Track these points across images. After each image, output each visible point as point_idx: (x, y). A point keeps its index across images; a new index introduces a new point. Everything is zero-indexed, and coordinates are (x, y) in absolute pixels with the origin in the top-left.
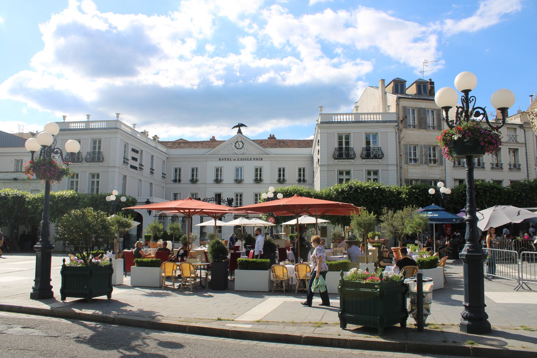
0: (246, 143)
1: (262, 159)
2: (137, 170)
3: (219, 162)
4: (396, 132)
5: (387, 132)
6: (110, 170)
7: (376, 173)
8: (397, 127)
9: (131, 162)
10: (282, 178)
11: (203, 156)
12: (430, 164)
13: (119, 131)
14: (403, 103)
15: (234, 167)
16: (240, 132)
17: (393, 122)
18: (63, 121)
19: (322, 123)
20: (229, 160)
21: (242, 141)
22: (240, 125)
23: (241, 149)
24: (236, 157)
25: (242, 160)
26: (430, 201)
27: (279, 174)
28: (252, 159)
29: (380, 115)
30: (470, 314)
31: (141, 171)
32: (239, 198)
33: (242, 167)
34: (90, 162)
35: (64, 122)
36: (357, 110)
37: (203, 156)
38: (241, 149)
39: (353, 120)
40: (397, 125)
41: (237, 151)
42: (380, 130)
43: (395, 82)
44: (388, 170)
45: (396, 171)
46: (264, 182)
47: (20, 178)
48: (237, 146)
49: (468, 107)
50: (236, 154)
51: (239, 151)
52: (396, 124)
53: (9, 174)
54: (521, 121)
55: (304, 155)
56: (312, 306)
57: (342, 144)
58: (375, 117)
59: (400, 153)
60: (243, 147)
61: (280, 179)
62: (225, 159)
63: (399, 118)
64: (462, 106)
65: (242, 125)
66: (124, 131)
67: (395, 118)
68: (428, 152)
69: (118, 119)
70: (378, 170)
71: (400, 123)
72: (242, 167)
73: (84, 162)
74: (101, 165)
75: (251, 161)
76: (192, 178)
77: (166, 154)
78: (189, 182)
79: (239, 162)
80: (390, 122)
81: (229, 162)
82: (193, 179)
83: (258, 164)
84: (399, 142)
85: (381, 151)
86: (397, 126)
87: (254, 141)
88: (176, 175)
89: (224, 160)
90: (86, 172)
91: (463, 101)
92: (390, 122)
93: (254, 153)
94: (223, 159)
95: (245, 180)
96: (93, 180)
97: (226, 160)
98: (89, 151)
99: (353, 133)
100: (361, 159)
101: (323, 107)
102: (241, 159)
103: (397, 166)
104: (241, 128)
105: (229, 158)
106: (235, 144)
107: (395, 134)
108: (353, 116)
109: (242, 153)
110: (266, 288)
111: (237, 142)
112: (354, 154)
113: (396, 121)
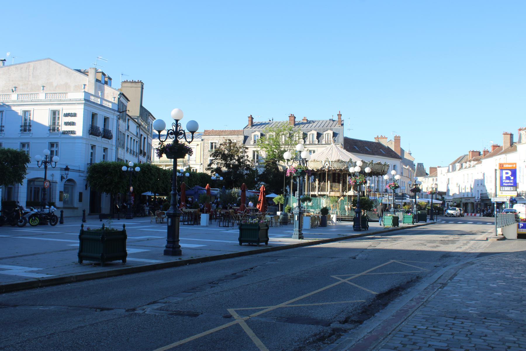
103: (116, 147)
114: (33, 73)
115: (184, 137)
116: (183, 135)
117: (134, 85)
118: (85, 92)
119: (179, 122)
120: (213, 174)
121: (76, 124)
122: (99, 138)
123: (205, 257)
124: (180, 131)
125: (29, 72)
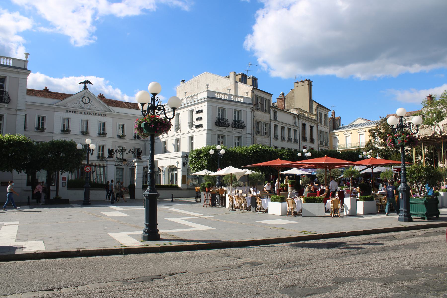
0: (92, 99)
1: (105, 115)
3: (67, 113)
5: (19, 78)
7: (223, 137)
10: (40, 126)
11: (52, 106)
12: (265, 136)
14: (256, 93)
15: (98, 121)
16: (85, 88)
20: (76, 112)
21: (89, 97)
23: (87, 104)
25: (88, 114)
27: (38, 122)
28: (97, 115)
30: (149, 230)
32: (101, 149)
36: (27, 57)
37: (52, 106)
38: (87, 104)
41: (83, 105)
45: (251, 138)
46: (107, 136)
48: (84, 101)
49: (402, 123)
50: (83, 108)
51: (85, 106)
52: (252, 106)
54: (297, 113)
55: (136, 116)
56: (303, 216)
58: (6, 62)
59: (253, 126)
60: (89, 102)
61: (39, 127)
62: (72, 111)
64: (399, 123)
67: (250, 102)
68: (265, 127)
70: (225, 135)
75: (96, 116)
78: (35, 130)
80: (248, 104)
83: (103, 119)
84: (253, 119)
85: (9, 95)
88: (39, 123)
89: (71, 112)
91: (400, 121)
92: (248, 104)
93: (99, 109)
99: (10, 77)
101: (29, 54)
102: (87, 114)
103: (252, 135)
104: (87, 84)
105: (76, 111)
106: (82, 99)
107: (251, 113)
109: (89, 108)
110: (325, 207)
111: (84, 97)
112: (229, 124)
114: (197, 86)
115: (163, 112)
116: (162, 110)
117: (303, 84)
118: (208, 91)
119: (156, 96)
120: (382, 153)
121: (203, 119)
122: (230, 129)
123: (114, 248)
124: (158, 105)
125: (195, 85)
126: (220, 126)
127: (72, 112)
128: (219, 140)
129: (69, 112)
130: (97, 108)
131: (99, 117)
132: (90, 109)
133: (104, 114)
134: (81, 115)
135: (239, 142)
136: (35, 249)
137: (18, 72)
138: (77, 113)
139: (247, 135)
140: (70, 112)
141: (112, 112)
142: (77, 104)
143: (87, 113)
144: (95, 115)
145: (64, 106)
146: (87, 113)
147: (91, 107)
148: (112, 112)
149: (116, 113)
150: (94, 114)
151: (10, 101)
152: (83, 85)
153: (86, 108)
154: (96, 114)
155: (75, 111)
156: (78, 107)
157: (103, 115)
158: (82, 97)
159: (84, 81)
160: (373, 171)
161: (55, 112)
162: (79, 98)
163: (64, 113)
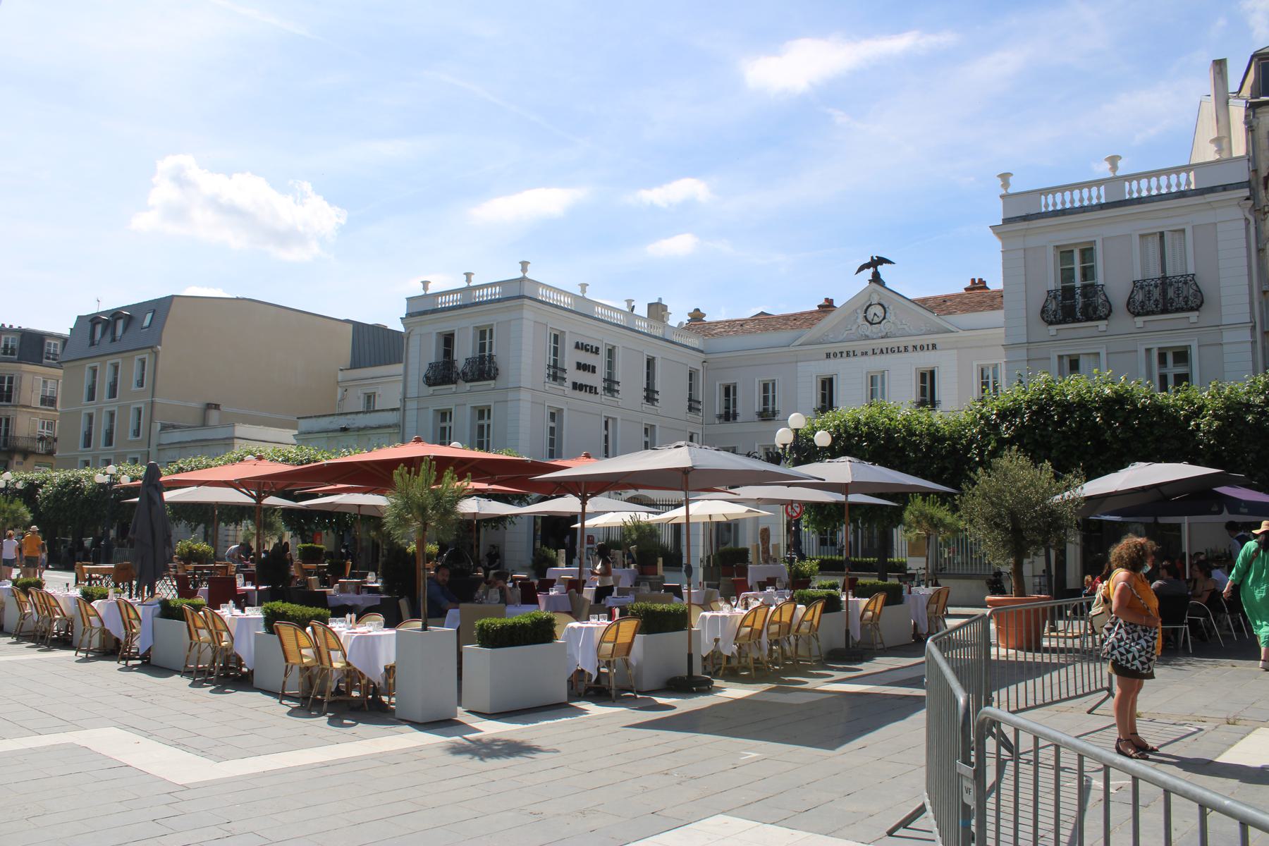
2: (596, 393)
3: (828, 361)
4: (1246, 219)
5: (1216, 224)
6: (511, 396)
7: (1182, 356)
8: (1251, 202)
9: (573, 375)
13: (526, 301)
15: (814, 376)
16: (876, 278)
17: (1237, 188)
18: (422, 293)
19: (1007, 221)
20: (851, 354)
22: (878, 262)
23: (880, 323)
24: (867, 345)
26: (831, 430)
29: (1192, 174)
31: (613, 396)
33: (884, 372)
34: (472, 381)
35: (425, 296)
39: (1103, 201)
40: (1248, 194)
42: (1189, 217)
43: (1260, 60)
44: (1221, 344)
45: (1250, 344)
47: (353, 426)
52: (1246, 192)
53: (336, 418)
57: (1072, 278)
62: (841, 353)
63: (1255, 171)
65: (882, 261)
66: (556, 306)
67: (1244, 176)
69: (527, 275)
71: (1261, 187)
72: (884, 372)
73: (460, 381)
74: (493, 386)
76: (764, 409)
77: (702, 352)
79: (877, 357)
80: (1225, 188)
81: (851, 359)
82: (765, 410)
83: (926, 360)
86: (1248, 199)
87: (922, 303)
89: (839, 355)
90: (465, 405)
94: (835, 355)
95: (943, 402)
96: (481, 422)
97: (844, 355)
98: (470, 356)
100: (1129, 317)
102: (848, 353)
103: (1254, 328)
108: (1102, 188)
109: (884, 334)
113: (1248, 184)
126: (1079, 321)
127: (841, 356)
128: (1164, 371)
129: (832, 356)
130: (910, 331)
131: (915, 354)
132: (888, 337)
133: (930, 342)
134: (865, 358)
135: (552, 424)
136: (638, 719)
137: (1209, 203)
138: (854, 355)
139: (1225, 334)
140: (835, 355)
141: (953, 332)
142: (853, 331)
143: (882, 350)
144: (903, 351)
145: (821, 343)
146: (882, 350)
147: (892, 330)
148: (953, 332)
149: (961, 331)
150: (902, 349)
151: (1202, 302)
152: (868, 273)
153: (875, 337)
154: (905, 349)
155: (847, 352)
156: (855, 338)
157: (928, 345)
158: (865, 308)
159: (869, 260)
160: (583, 508)
161: (799, 364)
162: (857, 313)
163: (821, 362)
